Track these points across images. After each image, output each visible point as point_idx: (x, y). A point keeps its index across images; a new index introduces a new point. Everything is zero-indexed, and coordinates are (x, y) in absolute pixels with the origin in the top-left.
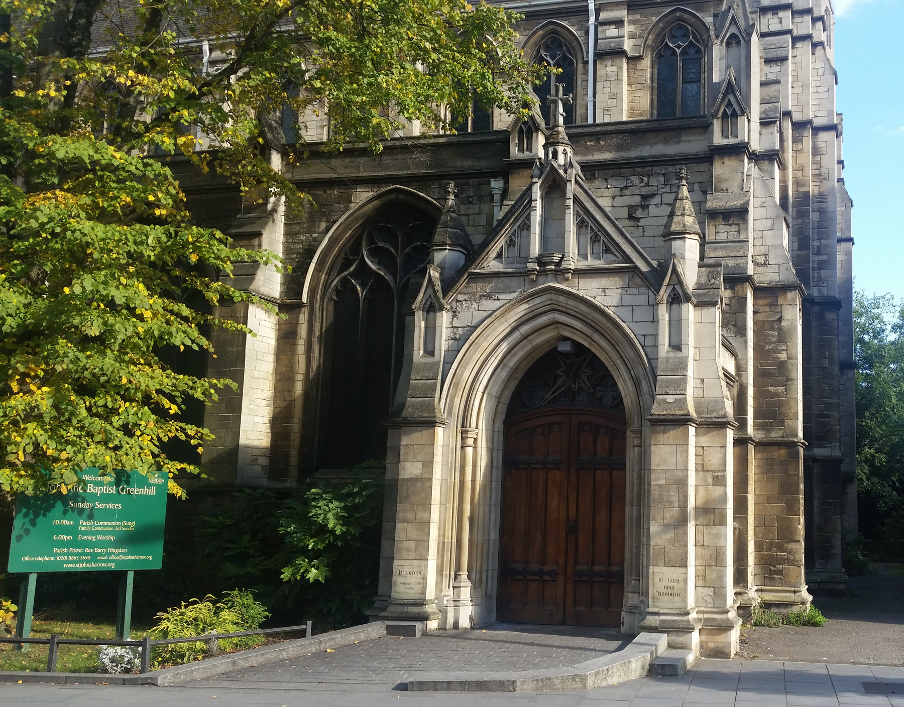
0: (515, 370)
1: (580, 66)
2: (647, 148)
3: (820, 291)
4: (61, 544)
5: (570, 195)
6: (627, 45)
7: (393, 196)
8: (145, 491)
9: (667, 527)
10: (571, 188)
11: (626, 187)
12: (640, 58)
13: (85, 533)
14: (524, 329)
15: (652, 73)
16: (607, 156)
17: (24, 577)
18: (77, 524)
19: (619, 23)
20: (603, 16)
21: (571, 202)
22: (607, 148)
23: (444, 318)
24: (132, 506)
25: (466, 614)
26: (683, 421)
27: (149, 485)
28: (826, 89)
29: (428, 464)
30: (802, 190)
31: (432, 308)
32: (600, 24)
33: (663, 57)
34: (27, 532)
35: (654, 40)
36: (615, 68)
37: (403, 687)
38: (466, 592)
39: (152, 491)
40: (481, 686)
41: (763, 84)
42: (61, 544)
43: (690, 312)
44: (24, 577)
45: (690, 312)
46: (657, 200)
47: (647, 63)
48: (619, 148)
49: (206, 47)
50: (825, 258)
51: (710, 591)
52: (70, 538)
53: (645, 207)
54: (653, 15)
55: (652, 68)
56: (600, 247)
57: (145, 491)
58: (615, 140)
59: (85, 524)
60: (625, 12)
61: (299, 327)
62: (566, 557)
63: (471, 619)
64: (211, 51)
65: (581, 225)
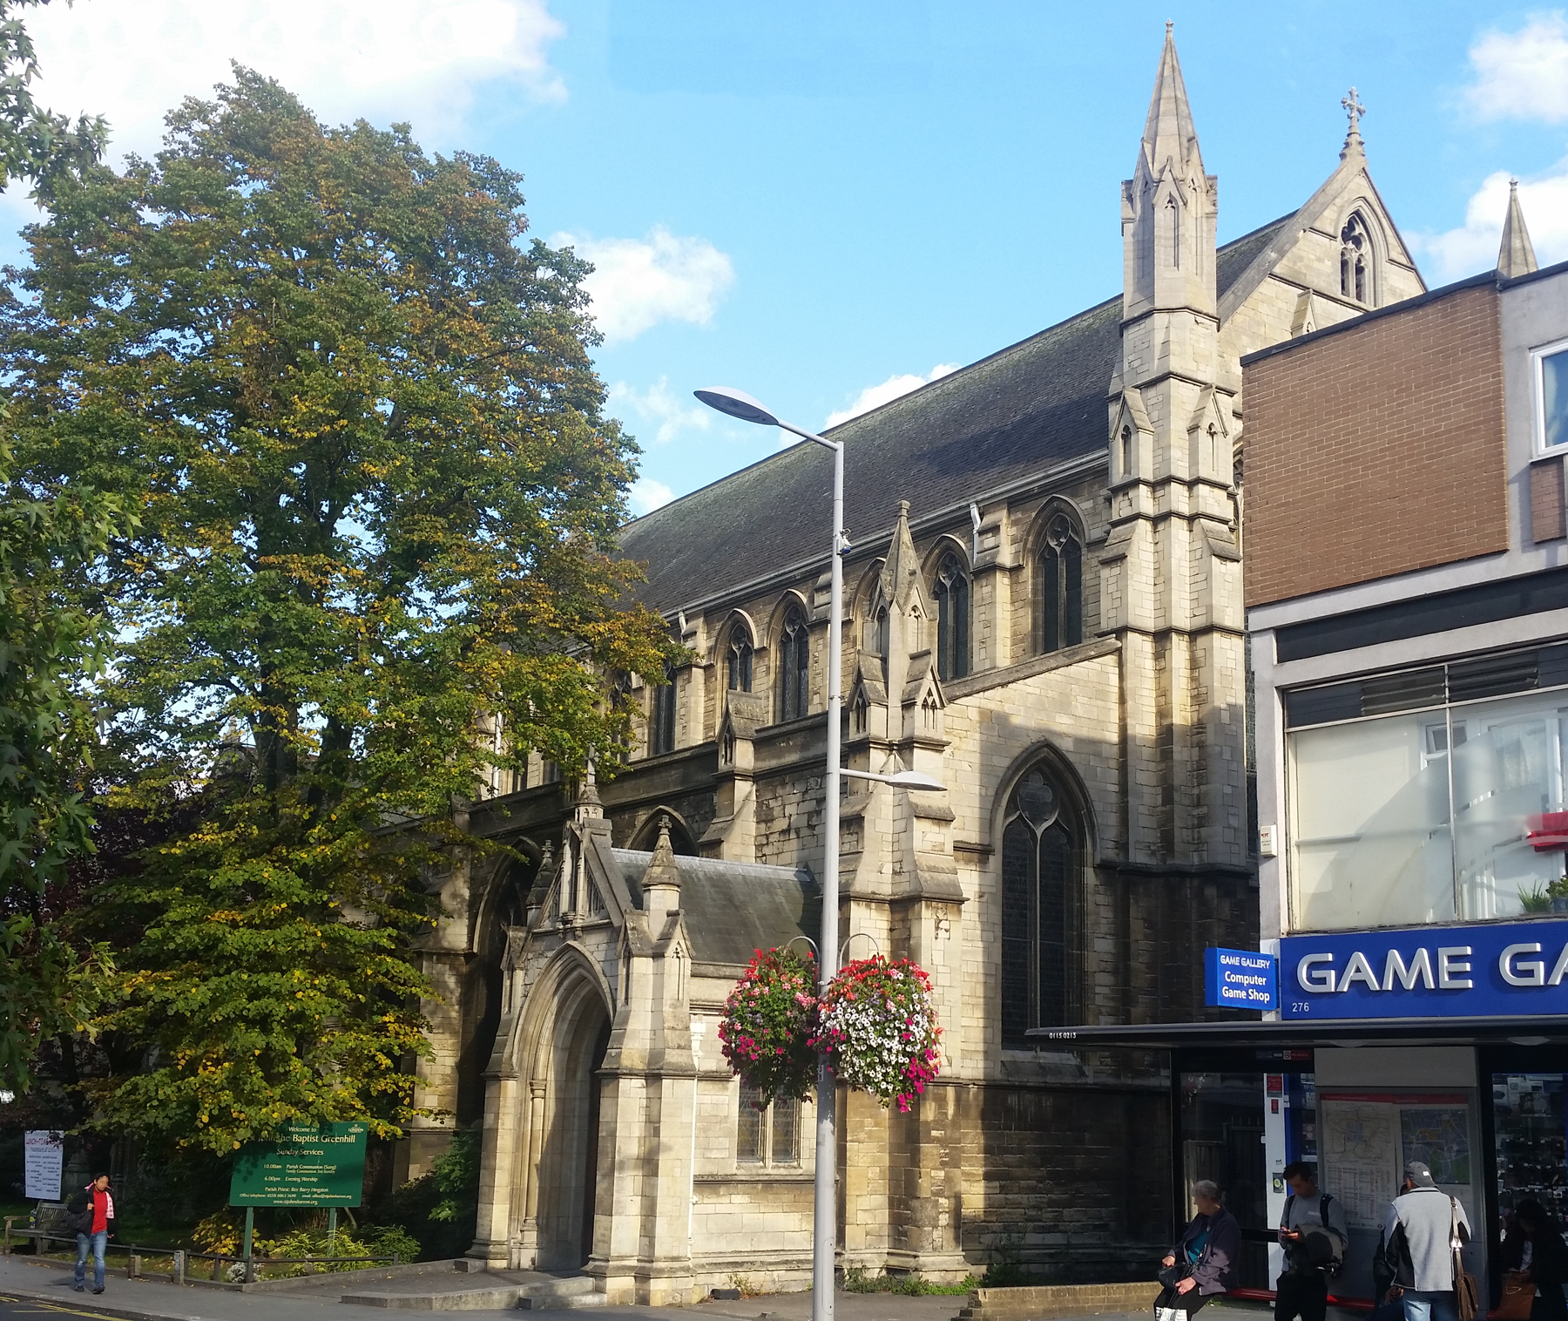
3: (1200, 856)
4: (271, 1184)
6: (1006, 557)
8: (345, 1139)
9: (604, 1176)
11: (806, 792)
12: (1019, 568)
13: (291, 1175)
14: (566, 983)
15: (1034, 584)
16: (792, 758)
17: (244, 1210)
18: (284, 1168)
22: (789, 750)
23: (519, 974)
24: (332, 1153)
25: (527, 1256)
27: (349, 1134)
28: (1203, 577)
30: (1165, 722)
31: (512, 969)
33: (1046, 562)
34: (250, 1173)
35: (1035, 542)
36: (989, 588)
37: (346, 1300)
38: (532, 1237)
39: (352, 1139)
42: (271, 1184)
44: (244, 1210)
47: (1028, 572)
48: (804, 747)
49: (975, 512)
50: (1204, 810)
52: (1529, 1245)
54: (1032, 510)
55: (1034, 577)
57: (345, 1139)
58: (799, 739)
59: (292, 1168)
60: (1005, 512)
61: (1265, 870)
63: (533, 1260)
64: (982, 516)
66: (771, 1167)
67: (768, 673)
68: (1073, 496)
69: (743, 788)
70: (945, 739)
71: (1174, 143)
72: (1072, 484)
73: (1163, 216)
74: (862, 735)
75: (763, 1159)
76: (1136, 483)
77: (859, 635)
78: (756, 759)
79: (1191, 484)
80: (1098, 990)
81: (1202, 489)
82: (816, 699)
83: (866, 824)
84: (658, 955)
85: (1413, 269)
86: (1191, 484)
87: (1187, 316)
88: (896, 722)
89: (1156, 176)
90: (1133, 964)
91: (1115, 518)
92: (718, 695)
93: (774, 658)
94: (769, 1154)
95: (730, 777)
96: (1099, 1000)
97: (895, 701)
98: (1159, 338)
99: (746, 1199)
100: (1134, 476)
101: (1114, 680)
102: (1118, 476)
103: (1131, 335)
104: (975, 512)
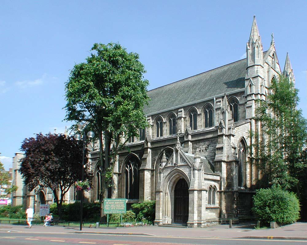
0: (174, 182)
1: (213, 111)
2: (208, 136)
5: (179, 153)
7: (167, 149)
10: (179, 151)
19: (220, 102)
20: (217, 100)
21: (179, 154)
23: (162, 174)
26: (194, 190)
29: (160, 198)
30: (15, 172)
31: (160, 173)
32: (216, 102)
40: (250, 238)
41: (229, 120)
43: (196, 172)
45: (196, 172)
46: (210, 146)
49: (215, 99)
51: (200, 218)
53: (208, 147)
56: (183, 161)
62: (181, 214)
65: (181, 158)
66: (212, 206)
67: (167, 126)
68: (236, 96)
69: (149, 150)
70: (235, 135)
71: (257, 37)
72: (236, 94)
73: (256, 49)
74: (221, 133)
75: (211, 204)
76: (253, 94)
77: (188, 119)
78: (151, 146)
79: (261, 95)
80: (248, 177)
81: (263, 96)
82: (179, 130)
83: (224, 148)
84: (199, 170)
85: (279, 64)
86: (261, 95)
87: (260, 66)
88: (227, 131)
89: (255, 42)
90: (252, 173)
91: (248, 100)
92: (155, 130)
93: (168, 124)
94: (212, 203)
95: (147, 148)
96: (248, 179)
97: (227, 128)
98: (256, 70)
99: (214, 210)
100: (252, 93)
101: (250, 127)
102: (249, 93)
103: (249, 70)
104: (215, 99)
